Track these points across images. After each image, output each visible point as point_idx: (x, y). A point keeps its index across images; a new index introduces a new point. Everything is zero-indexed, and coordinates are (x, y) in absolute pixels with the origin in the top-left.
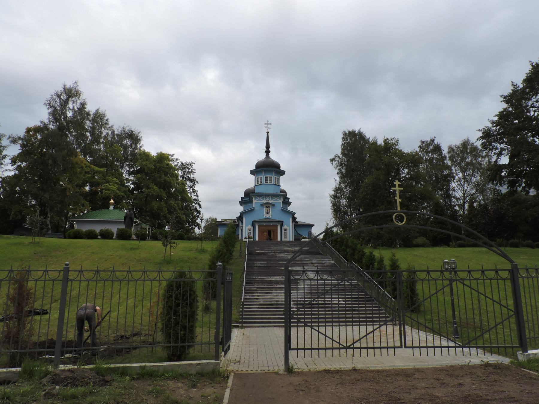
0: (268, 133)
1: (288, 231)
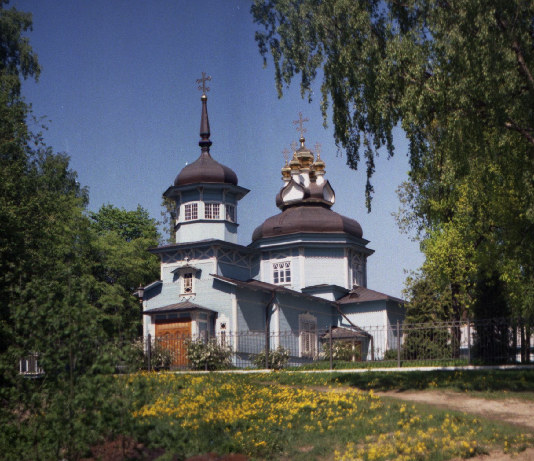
0: (204, 101)
1: (228, 326)
